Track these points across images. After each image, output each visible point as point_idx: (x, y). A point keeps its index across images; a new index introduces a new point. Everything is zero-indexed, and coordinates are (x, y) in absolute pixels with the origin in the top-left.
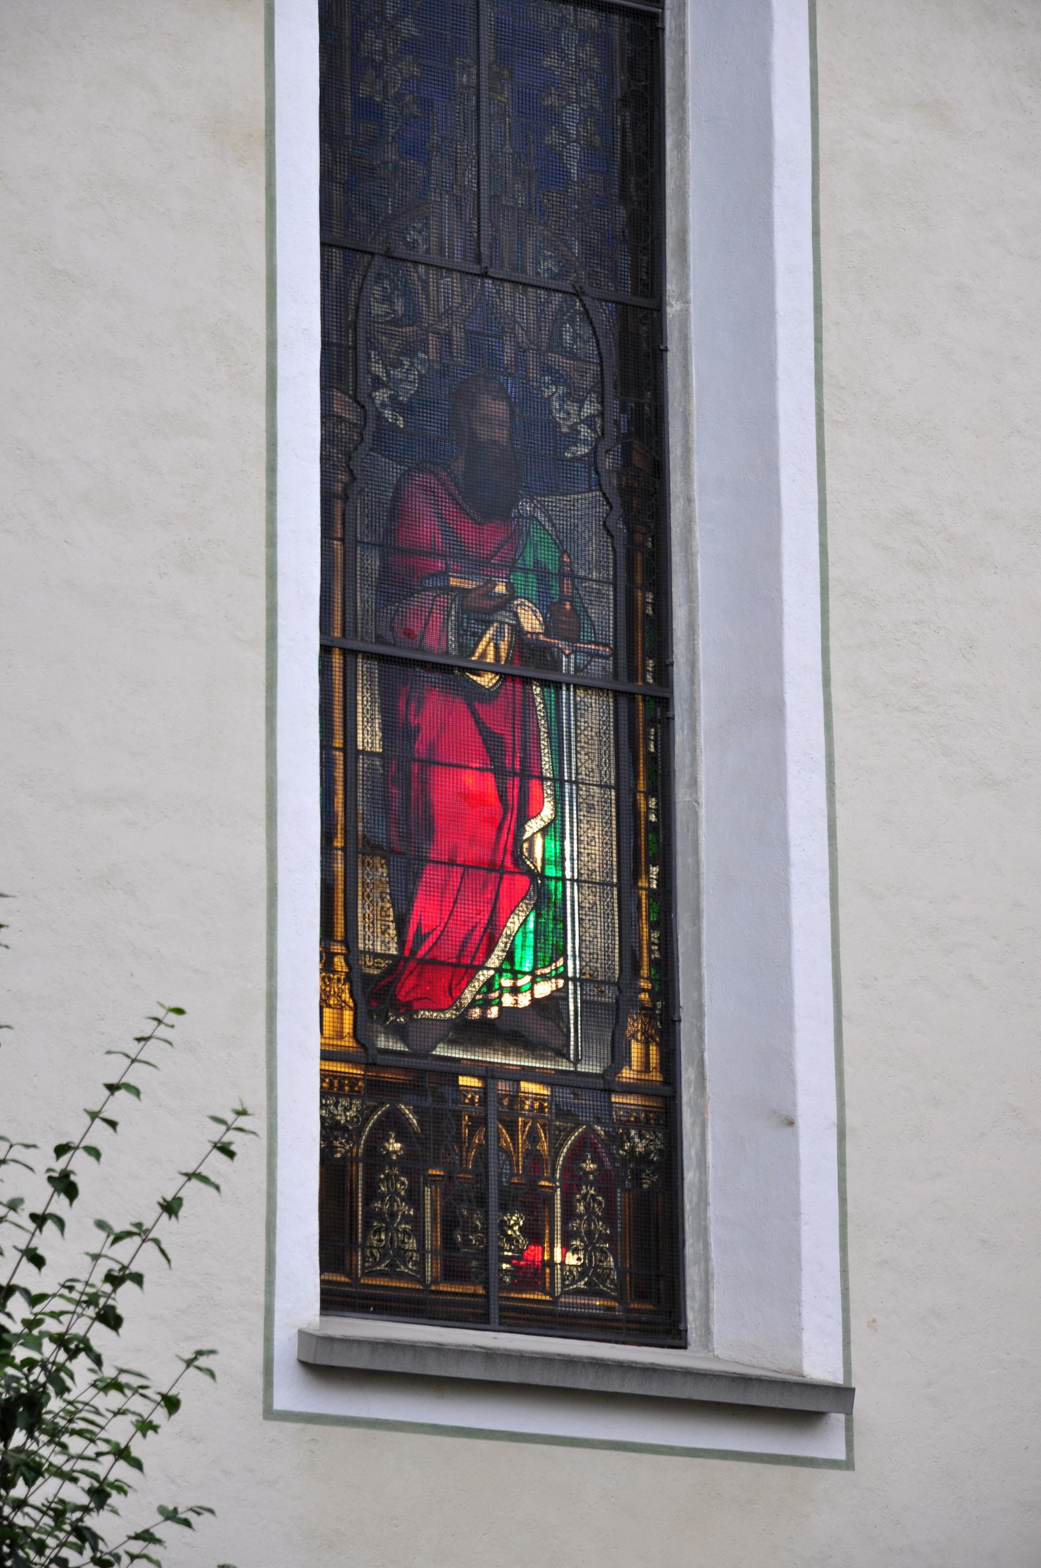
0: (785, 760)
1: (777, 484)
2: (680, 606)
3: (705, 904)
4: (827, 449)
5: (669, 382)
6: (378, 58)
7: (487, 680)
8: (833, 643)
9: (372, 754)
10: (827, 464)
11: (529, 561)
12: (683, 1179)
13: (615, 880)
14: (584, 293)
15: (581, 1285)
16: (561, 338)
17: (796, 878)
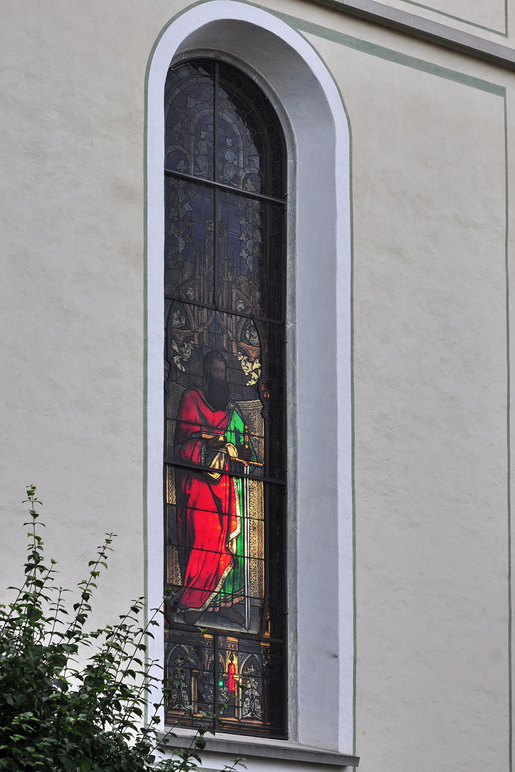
0: (337, 514)
1: (336, 402)
3: (298, 568)
6: (176, 219)
7: (216, 476)
9: (172, 505)
13: (263, 558)
15: (249, 715)
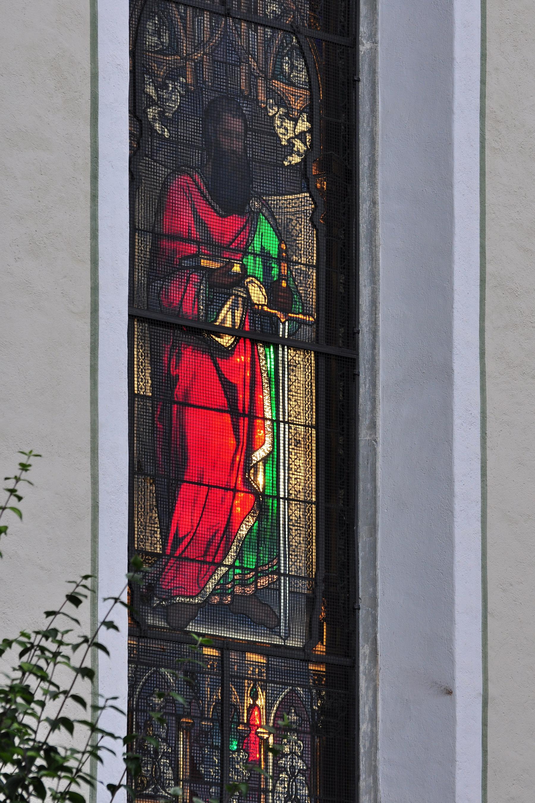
2: (365, 286)
3: (379, 520)
4: (487, 170)
5: (360, 107)
7: (226, 341)
8: (487, 323)
9: (145, 397)
10: (487, 182)
11: (258, 249)
12: (359, 729)
13: (314, 499)
14: (299, 32)
16: (282, 68)
17: (458, 505)
